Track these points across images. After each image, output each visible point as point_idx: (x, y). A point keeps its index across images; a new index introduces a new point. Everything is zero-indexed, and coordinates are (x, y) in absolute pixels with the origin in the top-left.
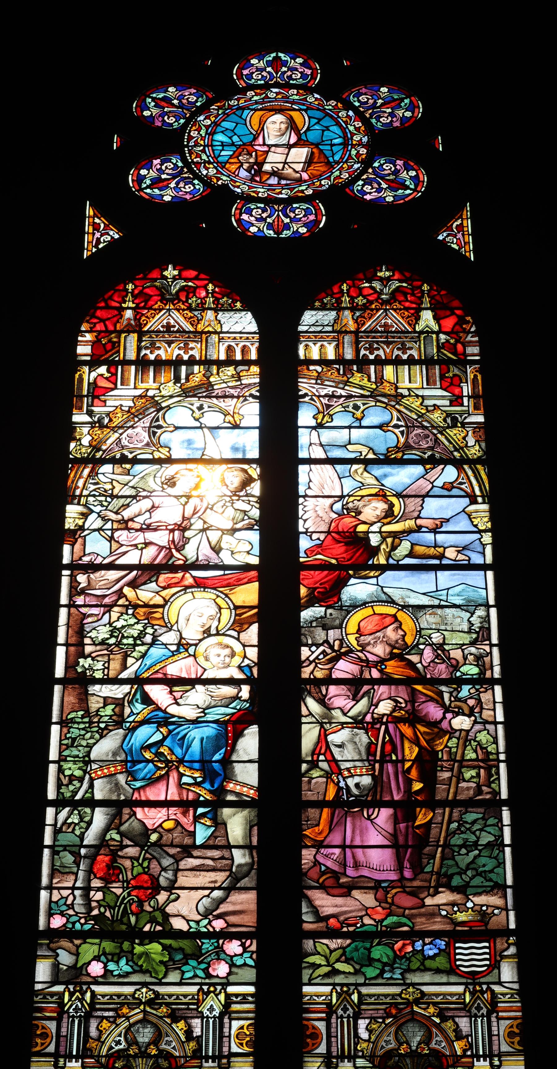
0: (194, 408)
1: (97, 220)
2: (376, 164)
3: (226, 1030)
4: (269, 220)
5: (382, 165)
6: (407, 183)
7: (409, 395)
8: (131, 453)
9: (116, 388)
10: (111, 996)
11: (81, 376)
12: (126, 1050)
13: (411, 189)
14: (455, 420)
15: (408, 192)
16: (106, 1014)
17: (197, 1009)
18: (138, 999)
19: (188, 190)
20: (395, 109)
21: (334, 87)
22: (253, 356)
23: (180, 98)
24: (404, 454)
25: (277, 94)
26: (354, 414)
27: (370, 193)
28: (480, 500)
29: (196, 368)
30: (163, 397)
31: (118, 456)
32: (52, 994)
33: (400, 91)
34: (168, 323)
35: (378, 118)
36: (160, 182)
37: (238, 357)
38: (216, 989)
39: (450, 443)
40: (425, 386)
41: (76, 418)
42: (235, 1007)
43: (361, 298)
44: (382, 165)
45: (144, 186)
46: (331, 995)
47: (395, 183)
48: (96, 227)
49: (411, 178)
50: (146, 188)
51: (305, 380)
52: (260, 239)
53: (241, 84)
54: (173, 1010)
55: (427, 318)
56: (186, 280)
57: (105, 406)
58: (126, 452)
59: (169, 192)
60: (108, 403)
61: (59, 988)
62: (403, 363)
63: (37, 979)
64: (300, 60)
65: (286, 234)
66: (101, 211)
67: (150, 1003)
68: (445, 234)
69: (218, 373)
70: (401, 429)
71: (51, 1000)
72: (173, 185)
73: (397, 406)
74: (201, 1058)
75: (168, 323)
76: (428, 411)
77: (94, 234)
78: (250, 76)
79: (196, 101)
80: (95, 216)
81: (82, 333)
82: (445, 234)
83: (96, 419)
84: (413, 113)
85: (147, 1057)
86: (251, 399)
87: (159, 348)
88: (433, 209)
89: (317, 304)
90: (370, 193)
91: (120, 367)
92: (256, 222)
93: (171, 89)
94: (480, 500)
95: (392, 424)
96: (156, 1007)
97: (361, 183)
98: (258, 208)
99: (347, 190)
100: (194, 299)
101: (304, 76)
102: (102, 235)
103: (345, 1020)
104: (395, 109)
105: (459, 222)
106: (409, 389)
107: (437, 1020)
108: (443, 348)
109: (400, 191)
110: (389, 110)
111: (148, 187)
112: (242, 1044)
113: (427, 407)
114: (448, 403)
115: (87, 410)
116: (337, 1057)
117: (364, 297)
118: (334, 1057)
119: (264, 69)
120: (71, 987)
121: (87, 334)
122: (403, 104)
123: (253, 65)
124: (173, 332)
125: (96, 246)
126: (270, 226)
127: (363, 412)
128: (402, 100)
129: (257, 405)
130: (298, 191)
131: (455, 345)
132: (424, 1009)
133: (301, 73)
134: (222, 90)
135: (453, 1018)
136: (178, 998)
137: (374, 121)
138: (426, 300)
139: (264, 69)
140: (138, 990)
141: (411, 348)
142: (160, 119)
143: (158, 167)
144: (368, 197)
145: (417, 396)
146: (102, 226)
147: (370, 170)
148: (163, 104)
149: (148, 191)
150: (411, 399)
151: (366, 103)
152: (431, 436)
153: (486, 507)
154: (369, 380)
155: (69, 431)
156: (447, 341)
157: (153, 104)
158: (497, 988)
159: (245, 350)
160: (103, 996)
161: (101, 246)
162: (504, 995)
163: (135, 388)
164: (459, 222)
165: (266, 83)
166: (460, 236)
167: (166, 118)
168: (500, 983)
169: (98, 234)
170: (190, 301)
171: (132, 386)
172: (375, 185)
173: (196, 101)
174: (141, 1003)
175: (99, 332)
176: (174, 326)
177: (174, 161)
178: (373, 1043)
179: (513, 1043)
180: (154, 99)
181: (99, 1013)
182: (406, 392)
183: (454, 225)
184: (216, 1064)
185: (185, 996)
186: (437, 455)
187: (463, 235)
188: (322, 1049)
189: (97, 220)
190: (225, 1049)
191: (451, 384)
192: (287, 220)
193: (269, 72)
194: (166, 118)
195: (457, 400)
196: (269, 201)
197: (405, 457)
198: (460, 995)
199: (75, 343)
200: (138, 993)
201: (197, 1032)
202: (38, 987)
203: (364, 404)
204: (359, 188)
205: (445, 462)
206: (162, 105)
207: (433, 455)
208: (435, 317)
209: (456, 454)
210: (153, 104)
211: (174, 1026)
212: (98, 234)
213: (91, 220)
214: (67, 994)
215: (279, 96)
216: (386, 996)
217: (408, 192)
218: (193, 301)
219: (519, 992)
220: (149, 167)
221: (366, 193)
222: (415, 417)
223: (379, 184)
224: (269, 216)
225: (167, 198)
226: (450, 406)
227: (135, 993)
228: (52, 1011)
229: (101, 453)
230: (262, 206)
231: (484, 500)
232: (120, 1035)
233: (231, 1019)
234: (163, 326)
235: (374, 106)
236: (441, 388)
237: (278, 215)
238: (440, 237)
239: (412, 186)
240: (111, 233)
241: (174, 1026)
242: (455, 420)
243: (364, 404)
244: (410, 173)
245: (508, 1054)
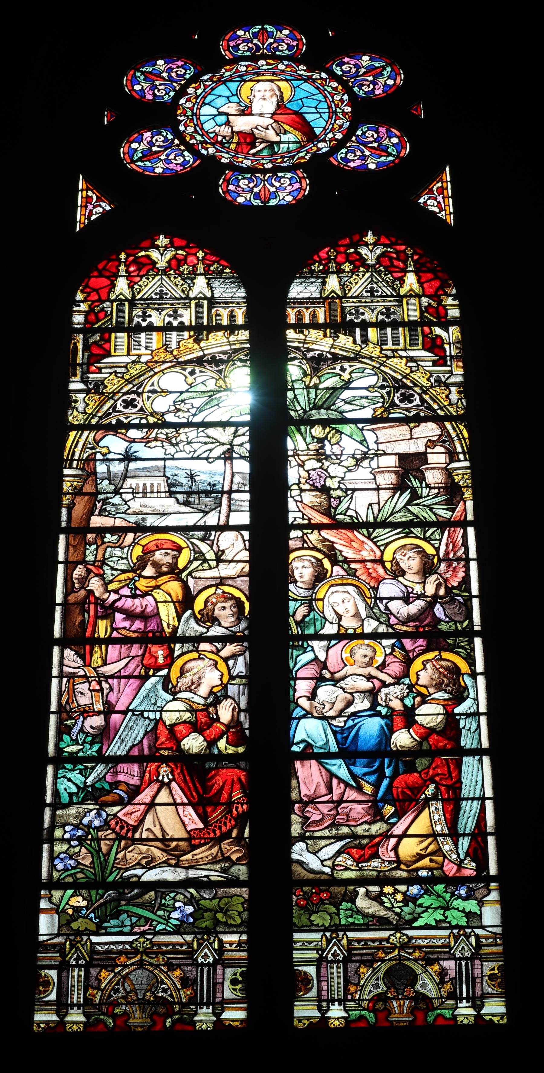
0: (186, 373)
1: (90, 193)
2: (359, 133)
3: (219, 976)
4: (271, 40)
5: (364, 133)
6: (390, 150)
7: (394, 357)
8: (126, 418)
9: (109, 355)
10: (303, 942)
11: (75, 344)
12: (386, 993)
13: (394, 156)
14: (438, 379)
15: (391, 158)
16: (364, 958)
17: (449, 953)
18: (392, 944)
19: (179, 162)
20: (378, 77)
21: (316, 58)
22: (240, 320)
23: (169, 70)
24: (389, 413)
25: (247, 66)
26: (340, 375)
27: (353, 161)
28: (461, 457)
29: (186, 334)
30: (156, 362)
31: (114, 422)
32: (54, 945)
33: (381, 58)
34: (161, 291)
35: (360, 87)
36: (154, 154)
37: (307, 320)
38: (338, 936)
39: (434, 401)
40: (408, 347)
41: (73, 386)
42: (485, 950)
43: (347, 264)
44: (364, 133)
45: (135, 158)
46: (449, 938)
47: (376, 150)
48: (88, 199)
49: (394, 145)
50: (137, 161)
51: (407, 333)
52: (247, 207)
53: (228, 56)
54: (426, 953)
55: (411, 279)
56: (177, 249)
57: (100, 373)
58: (122, 418)
59: (160, 164)
60: (103, 370)
61: (61, 939)
62: (388, 325)
63: (41, 932)
64: (286, 32)
65: (256, 29)
66: (93, 183)
67: (403, 947)
68: (426, 197)
69: (208, 339)
70: (387, 390)
71: (309, 947)
72: (163, 157)
73: (382, 368)
74: (196, 1004)
75: (161, 291)
76: (412, 372)
77: (86, 207)
78: (236, 47)
79: (185, 74)
80: (87, 189)
81: (77, 303)
82: (426, 197)
83: (91, 387)
84: (395, 81)
85: (144, 1004)
86: (238, 364)
87: (150, 316)
88: (410, 175)
89: (96, 274)
90: (353, 161)
91: (113, 335)
92: (283, 38)
93: (372, 166)
94: (461, 457)
95: (378, 385)
96: (411, 951)
97: (187, 76)
98: (245, 178)
99: (332, 159)
100: (186, 266)
101: (290, 48)
102: (95, 207)
103: (463, 963)
104: (378, 77)
105: (439, 184)
106: (394, 351)
107: (165, 969)
108: (427, 311)
109: (383, 158)
110: (371, 78)
111: (140, 159)
112: (494, 985)
113: (411, 367)
114: (431, 364)
115: (82, 378)
116: (328, 1001)
117: (351, 263)
118: (324, 1001)
119: (251, 41)
120: (328, 934)
121: (82, 304)
122: (385, 72)
123: (239, 37)
124: (377, 296)
125: (89, 218)
126: (257, 196)
127: (350, 374)
128: (384, 68)
129: (247, 370)
130: (299, 158)
131: (437, 308)
132: (410, 954)
133: (287, 44)
134: (210, 63)
135: (179, 966)
136: (303, 945)
137: (356, 89)
138: (122, 268)
139: (251, 41)
140: (136, 940)
141: (394, 313)
142: (151, 92)
143: (149, 139)
144: (352, 165)
145: (401, 357)
146: (95, 198)
147: (354, 138)
148: (152, 77)
149: (139, 163)
150: (395, 360)
151: (349, 71)
152: (416, 396)
153: (467, 464)
154: (354, 342)
155: (66, 401)
156: (429, 304)
157: (142, 77)
158: (480, 932)
159: (232, 315)
160: (231, 944)
161: (93, 218)
162: (486, 938)
163: (128, 354)
164: (439, 184)
165: (253, 54)
166: (439, 202)
167: (375, 136)
168: (482, 927)
169: (90, 207)
170: (181, 269)
171: (125, 353)
172: (359, 153)
173: (346, 153)
174: (394, 948)
175: (93, 302)
176: (167, 294)
177: (165, 134)
178: (102, 991)
179: (235, 990)
180: (143, 73)
181: (358, 958)
182: (390, 354)
183: (435, 189)
184: (210, 1011)
185: (310, 943)
186: (422, 414)
187: (443, 198)
188: (313, 993)
189: (90, 193)
190: (478, 989)
191: (434, 345)
192: (255, 41)
193: (255, 44)
194: (156, 91)
195: (441, 361)
196: (252, 171)
197: (391, 416)
198: (445, 938)
199: (71, 313)
200: (392, 938)
201: (452, 973)
202: (41, 938)
203: (351, 366)
204: (343, 156)
205: (426, 419)
206: (155, 80)
207: (418, 414)
208: (419, 281)
209: (439, 412)
210: (142, 77)
211: (169, 973)
212: (439, 202)
213: (84, 192)
214: (195, 943)
215: (250, 69)
216: (373, 940)
217: (391, 158)
218: (185, 268)
219: (503, 936)
220: (140, 142)
221: (182, 67)
222: (400, 377)
223: (362, 152)
224: (271, 44)
225: (366, 58)
226: (434, 366)
227: (389, 938)
228: (55, 961)
229: (97, 419)
230: (278, 53)
231: (465, 457)
232: (117, 984)
233: (224, 968)
234: (156, 294)
235: (356, 75)
236: (424, 349)
237: (264, 185)
238: (422, 200)
239: (395, 153)
240: (103, 204)
241: (169, 973)
242: (438, 379)
243: (351, 366)
244: (140, 87)
245: (491, 996)
